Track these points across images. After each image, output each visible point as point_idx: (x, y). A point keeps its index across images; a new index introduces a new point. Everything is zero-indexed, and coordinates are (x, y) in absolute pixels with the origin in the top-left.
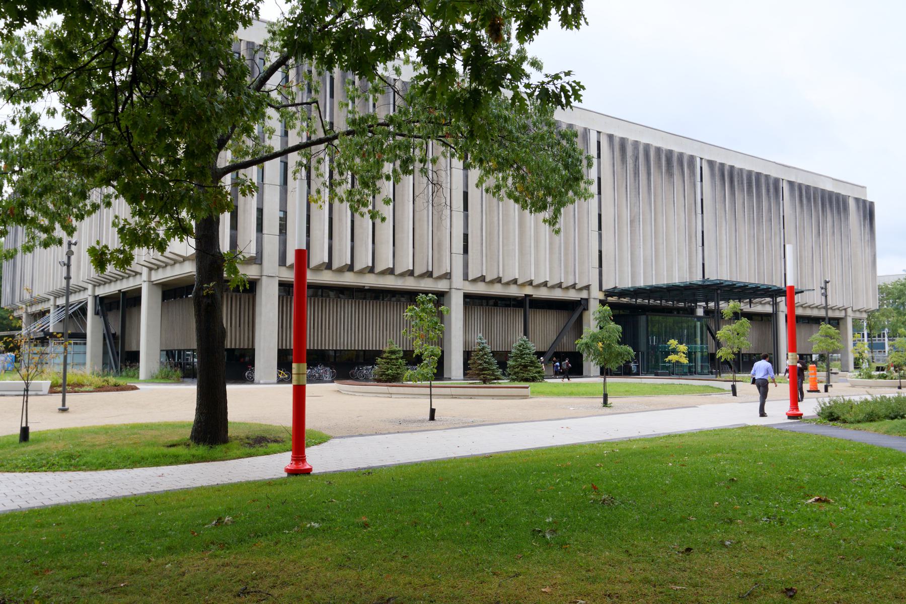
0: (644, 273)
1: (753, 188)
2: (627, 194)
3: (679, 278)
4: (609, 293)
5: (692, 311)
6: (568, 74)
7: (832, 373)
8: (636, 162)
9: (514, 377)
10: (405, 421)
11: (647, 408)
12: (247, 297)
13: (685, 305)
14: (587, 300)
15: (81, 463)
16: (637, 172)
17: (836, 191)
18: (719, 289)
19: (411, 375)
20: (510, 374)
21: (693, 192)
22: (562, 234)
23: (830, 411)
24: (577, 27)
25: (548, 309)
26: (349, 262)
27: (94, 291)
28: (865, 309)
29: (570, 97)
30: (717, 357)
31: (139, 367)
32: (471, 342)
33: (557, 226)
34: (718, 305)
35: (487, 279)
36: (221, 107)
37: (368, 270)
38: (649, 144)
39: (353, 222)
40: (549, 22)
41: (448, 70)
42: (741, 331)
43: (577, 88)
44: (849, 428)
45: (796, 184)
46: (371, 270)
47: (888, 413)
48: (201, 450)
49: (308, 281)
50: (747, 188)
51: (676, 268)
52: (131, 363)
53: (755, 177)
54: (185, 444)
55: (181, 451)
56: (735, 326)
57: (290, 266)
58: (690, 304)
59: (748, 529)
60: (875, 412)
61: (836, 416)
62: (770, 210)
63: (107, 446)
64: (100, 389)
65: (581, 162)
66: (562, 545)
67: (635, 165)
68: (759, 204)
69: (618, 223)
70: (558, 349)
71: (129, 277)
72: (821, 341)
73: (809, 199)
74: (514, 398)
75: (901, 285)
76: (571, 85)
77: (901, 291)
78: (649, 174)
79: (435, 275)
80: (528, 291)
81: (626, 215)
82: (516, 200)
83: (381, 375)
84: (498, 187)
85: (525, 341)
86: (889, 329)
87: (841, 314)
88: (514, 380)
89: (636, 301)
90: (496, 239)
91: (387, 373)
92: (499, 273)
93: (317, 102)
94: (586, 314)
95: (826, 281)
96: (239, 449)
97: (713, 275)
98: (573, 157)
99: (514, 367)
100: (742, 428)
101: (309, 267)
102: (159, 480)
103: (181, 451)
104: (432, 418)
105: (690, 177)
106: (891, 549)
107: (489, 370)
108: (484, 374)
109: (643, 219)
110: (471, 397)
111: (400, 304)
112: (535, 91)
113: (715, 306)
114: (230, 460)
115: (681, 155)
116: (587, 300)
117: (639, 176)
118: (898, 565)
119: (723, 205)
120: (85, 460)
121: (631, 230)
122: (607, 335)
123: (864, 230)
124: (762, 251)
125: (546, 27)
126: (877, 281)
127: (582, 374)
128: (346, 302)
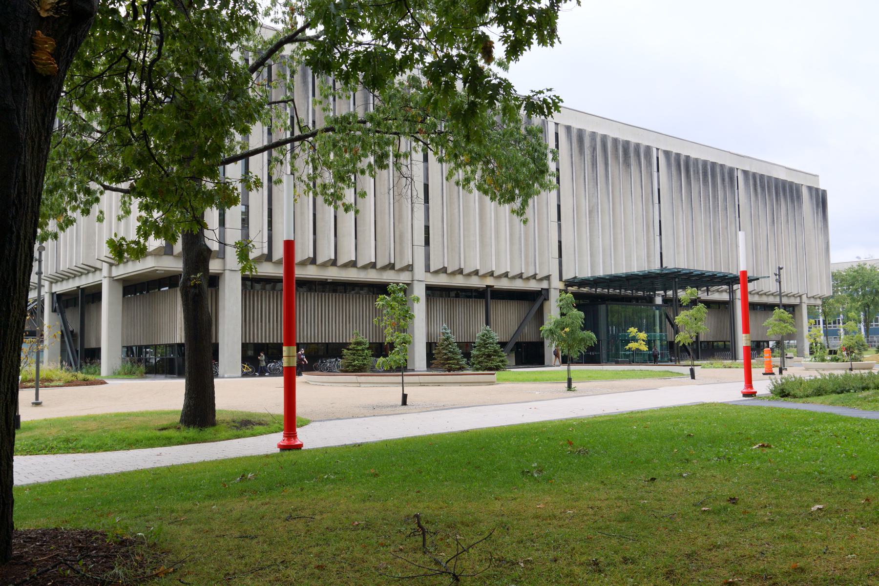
0: (604, 263)
1: (708, 177)
2: (585, 185)
3: (637, 267)
4: (569, 283)
5: (650, 300)
6: (550, 90)
7: (787, 358)
8: (593, 153)
9: (478, 366)
10: (378, 406)
12: (313, 295)
13: (644, 294)
14: (547, 290)
15: (79, 446)
16: (595, 164)
17: (789, 179)
18: (676, 277)
19: (384, 362)
21: (650, 181)
23: (781, 388)
24: (552, 45)
26: (312, 256)
27: (51, 288)
29: (551, 108)
30: (676, 342)
31: (100, 363)
34: (676, 293)
35: (449, 271)
36: (234, 112)
37: (331, 262)
41: (450, 86)
42: (699, 315)
43: (557, 101)
44: (798, 402)
45: (751, 174)
46: (334, 263)
47: (834, 389)
48: (192, 432)
49: (296, 276)
52: (91, 360)
58: (648, 293)
59: (701, 466)
61: (787, 392)
62: (725, 199)
63: (100, 430)
64: (69, 384)
65: (546, 155)
66: (548, 480)
67: (593, 156)
69: (577, 213)
70: (519, 340)
71: (88, 273)
72: (775, 325)
73: (763, 188)
75: (854, 272)
76: (552, 99)
77: (854, 277)
79: (397, 267)
80: (490, 282)
81: (585, 206)
83: (348, 366)
84: (467, 180)
86: (844, 316)
87: (796, 301)
88: (477, 369)
89: (596, 291)
90: (457, 231)
91: (353, 364)
93: (293, 100)
94: (546, 304)
95: (779, 267)
97: (671, 264)
98: (539, 151)
99: (477, 356)
100: (700, 405)
102: (159, 458)
104: (404, 403)
105: (647, 167)
106: (816, 473)
107: (454, 359)
108: (449, 364)
109: (601, 209)
110: (439, 384)
111: (359, 296)
112: (522, 103)
113: (673, 294)
115: (637, 146)
116: (547, 290)
117: (597, 167)
118: (820, 483)
119: (680, 195)
120: (82, 443)
121: (589, 221)
122: (570, 321)
123: (817, 217)
125: (530, 49)
126: (831, 269)
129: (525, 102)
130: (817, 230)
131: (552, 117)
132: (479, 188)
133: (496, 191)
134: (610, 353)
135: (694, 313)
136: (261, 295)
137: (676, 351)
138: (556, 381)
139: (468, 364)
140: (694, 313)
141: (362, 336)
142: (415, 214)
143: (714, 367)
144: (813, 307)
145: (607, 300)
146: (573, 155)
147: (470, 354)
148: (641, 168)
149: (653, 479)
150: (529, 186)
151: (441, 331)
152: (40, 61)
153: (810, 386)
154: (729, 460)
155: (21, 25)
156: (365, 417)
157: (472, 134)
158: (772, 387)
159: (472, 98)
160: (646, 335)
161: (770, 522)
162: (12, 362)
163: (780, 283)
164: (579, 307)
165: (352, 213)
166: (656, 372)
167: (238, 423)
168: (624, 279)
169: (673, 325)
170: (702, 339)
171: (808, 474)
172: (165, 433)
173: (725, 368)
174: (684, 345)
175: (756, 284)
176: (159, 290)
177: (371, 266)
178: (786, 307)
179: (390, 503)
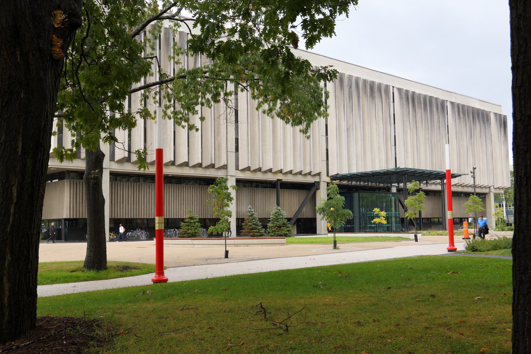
0: (357, 164)
2: (344, 111)
4: (334, 178)
5: (388, 190)
6: (332, 66)
9: (272, 234)
11: (362, 249)
13: (384, 185)
14: (318, 183)
16: (351, 97)
17: (482, 108)
19: (213, 229)
22: (311, 138)
24: (331, 37)
28: (502, 187)
32: (243, 212)
33: (308, 134)
34: (406, 185)
35: (252, 169)
37: (171, 163)
38: (358, 77)
39: (188, 133)
40: (320, 40)
43: (335, 72)
44: (483, 254)
47: (505, 246)
48: (92, 273)
49: (164, 173)
50: (423, 107)
51: (377, 161)
54: (81, 270)
55: (79, 274)
56: (417, 197)
57: (117, 161)
60: (498, 245)
66: (329, 289)
67: (350, 91)
68: (432, 116)
70: (299, 217)
73: (464, 114)
78: (359, 97)
79: (216, 166)
80: (280, 177)
82: (283, 118)
83: (184, 234)
84: (271, 110)
89: (352, 183)
91: (188, 232)
94: (318, 192)
96: (114, 273)
97: (402, 165)
99: (271, 227)
103: (79, 274)
104: (226, 256)
105: (386, 99)
107: (256, 229)
108: (253, 232)
110: (248, 245)
112: (316, 73)
113: (404, 185)
114: (111, 279)
115: (380, 85)
116: (318, 183)
117: (352, 99)
119: (408, 118)
124: (434, 149)
125: (319, 42)
129: (317, 73)
130: (501, 143)
131: (333, 81)
133: (289, 118)
135: (417, 198)
136: (123, 185)
137: (405, 224)
138: (326, 243)
139: (265, 232)
140: (417, 198)
141: (194, 213)
143: (431, 235)
144: (498, 195)
146: (336, 91)
147: (267, 226)
148: (382, 99)
149: (389, 288)
151: (248, 210)
153: (489, 244)
154: (433, 279)
155: (47, 33)
156: (202, 265)
158: (466, 245)
159: (287, 70)
160: (385, 213)
161: (452, 304)
162: (39, 217)
163: (474, 178)
164: (341, 194)
166: (392, 237)
167: (121, 267)
168: (360, 176)
169: (403, 206)
170: (423, 216)
171: (476, 285)
172: (74, 273)
173: (438, 235)
174: (410, 219)
176: (51, 181)
177: (269, 171)
178: (478, 194)
179: (240, 301)
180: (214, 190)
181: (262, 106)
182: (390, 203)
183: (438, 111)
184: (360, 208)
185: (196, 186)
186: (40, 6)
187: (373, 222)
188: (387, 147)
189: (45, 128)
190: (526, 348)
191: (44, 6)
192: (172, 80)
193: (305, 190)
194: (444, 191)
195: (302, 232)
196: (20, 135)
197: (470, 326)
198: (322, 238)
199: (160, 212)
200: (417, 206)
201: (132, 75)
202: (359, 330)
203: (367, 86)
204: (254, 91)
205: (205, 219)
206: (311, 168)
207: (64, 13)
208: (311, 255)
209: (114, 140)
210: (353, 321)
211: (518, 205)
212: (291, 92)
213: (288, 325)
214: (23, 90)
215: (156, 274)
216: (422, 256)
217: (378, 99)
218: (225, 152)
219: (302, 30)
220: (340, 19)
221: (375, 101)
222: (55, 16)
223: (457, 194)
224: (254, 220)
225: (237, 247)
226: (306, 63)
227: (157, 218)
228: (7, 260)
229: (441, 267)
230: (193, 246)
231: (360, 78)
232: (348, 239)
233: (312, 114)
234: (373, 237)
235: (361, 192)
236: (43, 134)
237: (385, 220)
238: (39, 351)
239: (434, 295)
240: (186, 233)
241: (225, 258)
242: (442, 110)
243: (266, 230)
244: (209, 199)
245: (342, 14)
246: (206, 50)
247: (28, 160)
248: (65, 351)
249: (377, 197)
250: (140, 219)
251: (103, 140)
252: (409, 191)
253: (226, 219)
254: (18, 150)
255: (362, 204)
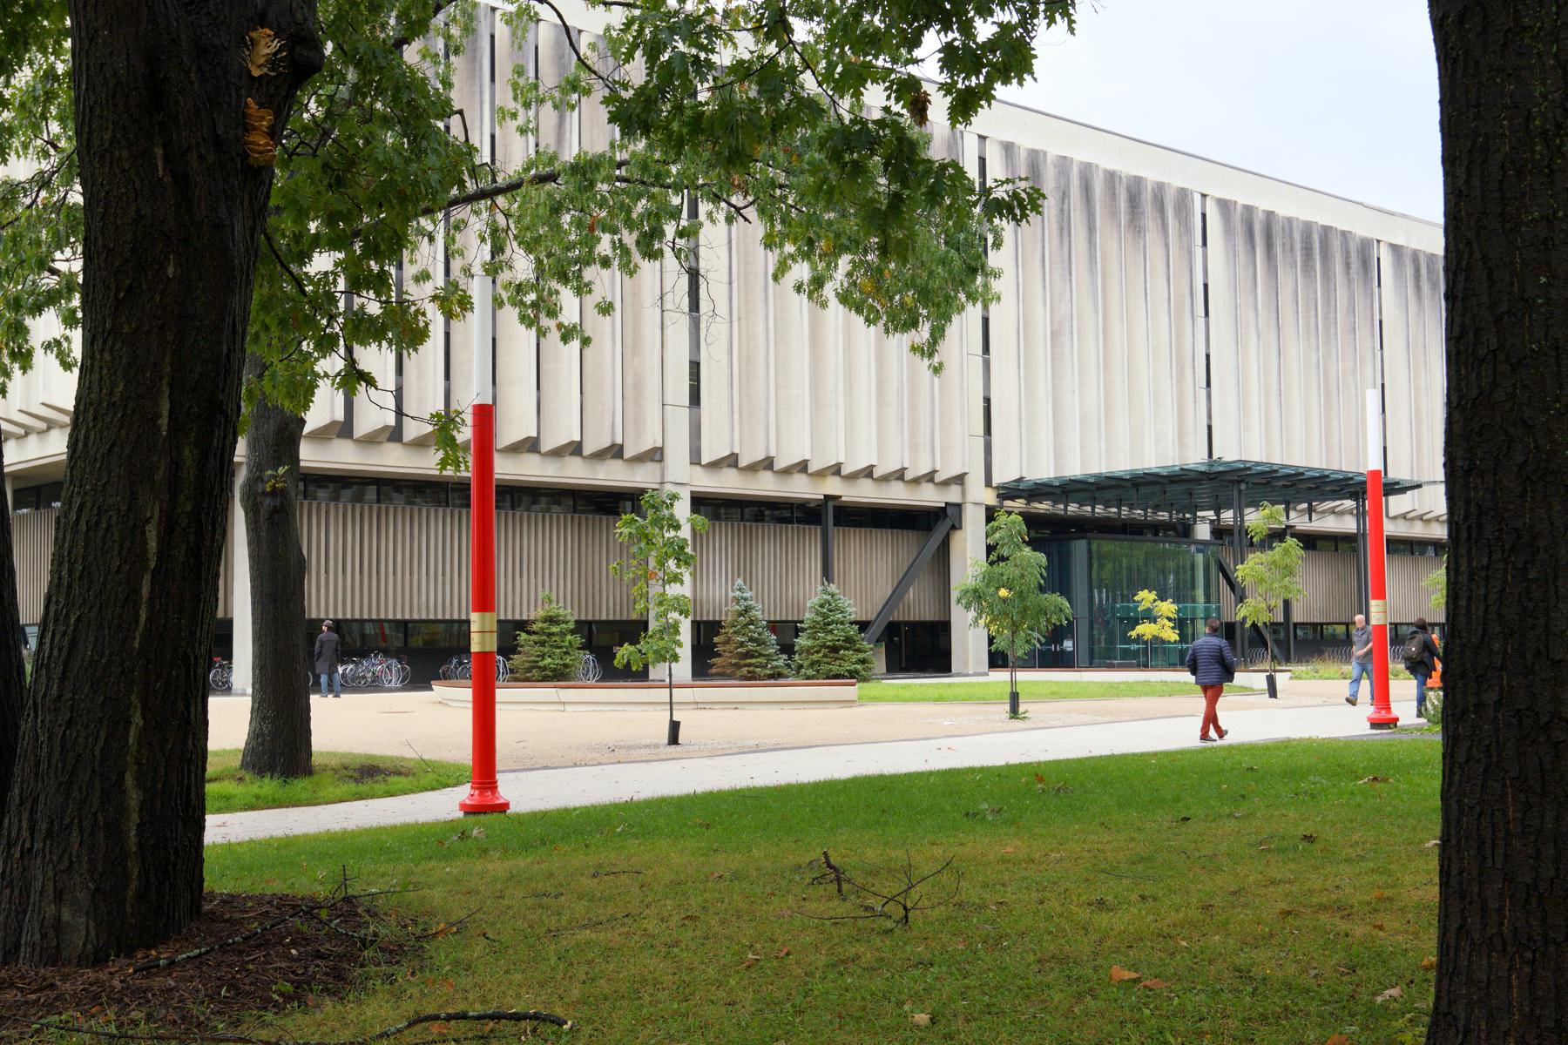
0: (1083, 447)
2: (1044, 274)
4: (1008, 492)
5: (1185, 531)
9: (810, 672)
11: (1099, 719)
12: (456, 516)
13: (1171, 516)
14: (959, 506)
16: (1066, 227)
18: (1242, 481)
19: (631, 653)
20: (801, 667)
24: (1020, 83)
25: (874, 527)
33: (936, 359)
34: (1242, 516)
35: (743, 462)
37: (387, 435)
39: (538, 345)
43: (1035, 196)
49: (496, 476)
50: (1303, 261)
53: (1320, 237)
54: (233, 777)
57: (309, 433)
66: (1013, 822)
67: (1062, 210)
68: (1329, 290)
69: (1026, 337)
70: (897, 616)
74: (825, 705)
78: (1091, 229)
79: (628, 454)
80: (833, 487)
83: (529, 670)
84: (818, 282)
85: (833, 596)
92: (768, 448)
94: (957, 540)
97: (1228, 452)
99: (809, 651)
101: (1387, 516)
104: (674, 739)
105: (1180, 236)
107: (760, 655)
108: (750, 665)
110: (736, 705)
113: (1235, 517)
114: (326, 804)
115: (1160, 189)
116: (959, 506)
117: (1070, 235)
121: (1052, 354)
125: (989, 105)
127: (950, 670)
128: (432, 514)
131: (1028, 222)
132: (844, 298)
134: (1096, 647)
136: (327, 513)
138: (985, 700)
139: (788, 666)
140: (1277, 557)
142: (669, 331)
143: (1321, 678)
145: (1090, 531)
148: (1166, 237)
150: (949, 301)
151: (731, 595)
152: (257, 148)
155: (234, 94)
156: (600, 764)
157: (892, 244)
160: (1174, 607)
164: (1035, 544)
165: (575, 344)
167: (354, 770)
168: (1093, 488)
169: (1232, 585)
170: (1297, 617)
174: (1254, 625)
175: (1416, 497)
177: (799, 468)
180: (633, 531)
181: (790, 267)
182: (1189, 573)
183: (1348, 274)
184: (1091, 591)
185: (555, 516)
186: (215, 18)
187: (1133, 634)
188: (1181, 392)
189: (229, 361)
190: (1463, 872)
191: (226, 17)
192: (513, 187)
193: (915, 532)
194: (1364, 535)
195: (904, 666)
196: (166, 379)
197: (1403, 910)
198: (971, 685)
199: (484, 601)
200: (1276, 585)
201: (423, 189)
202: (1103, 920)
203: (1117, 191)
204: (773, 226)
205: (590, 623)
206: (934, 457)
207: (276, 36)
208: (938, 738)
209: (366, 381)
210: (1084, 898)
211: (1452, 581)
212: (907, 250)
213: (909, 905)
214: (171, 257)
215: (472, 788)
216: (1289, 740)
217: (1152, 237)
218: (658, 405)
219: (942, 72)
220: (1047, 39)
221: (1145, 240)
222: (252, 44)
223: (1408, 547)
224: (752, 627)
225: (703, 712)
226: (951, 171)
227: (475, 617)
228: (134, 727)
229: (1339, 765)
230: (561, 707)
231: (1097, 166)
232: (1054, 689)
233: (950, 296)
234: (1134, 683)
235: (1094, 539)
236: (225, 378)
237: (1173, 628)
238: (230, 972)
239: (1311, 836)
240: (534, 667)
241: (670, 744)
242: (1361, 272)
243: (790, 658)
244: (618, 560)
245: (1056, 23)
246: (659, 127)
247: (187, 451)
248: (303, 974)
249: (1146, 553)
250: (373, 621)
251: (334, 381)
252: (1252, 537)
253: (670, 621)
254: (159, 422)
255: (1098, 575)
